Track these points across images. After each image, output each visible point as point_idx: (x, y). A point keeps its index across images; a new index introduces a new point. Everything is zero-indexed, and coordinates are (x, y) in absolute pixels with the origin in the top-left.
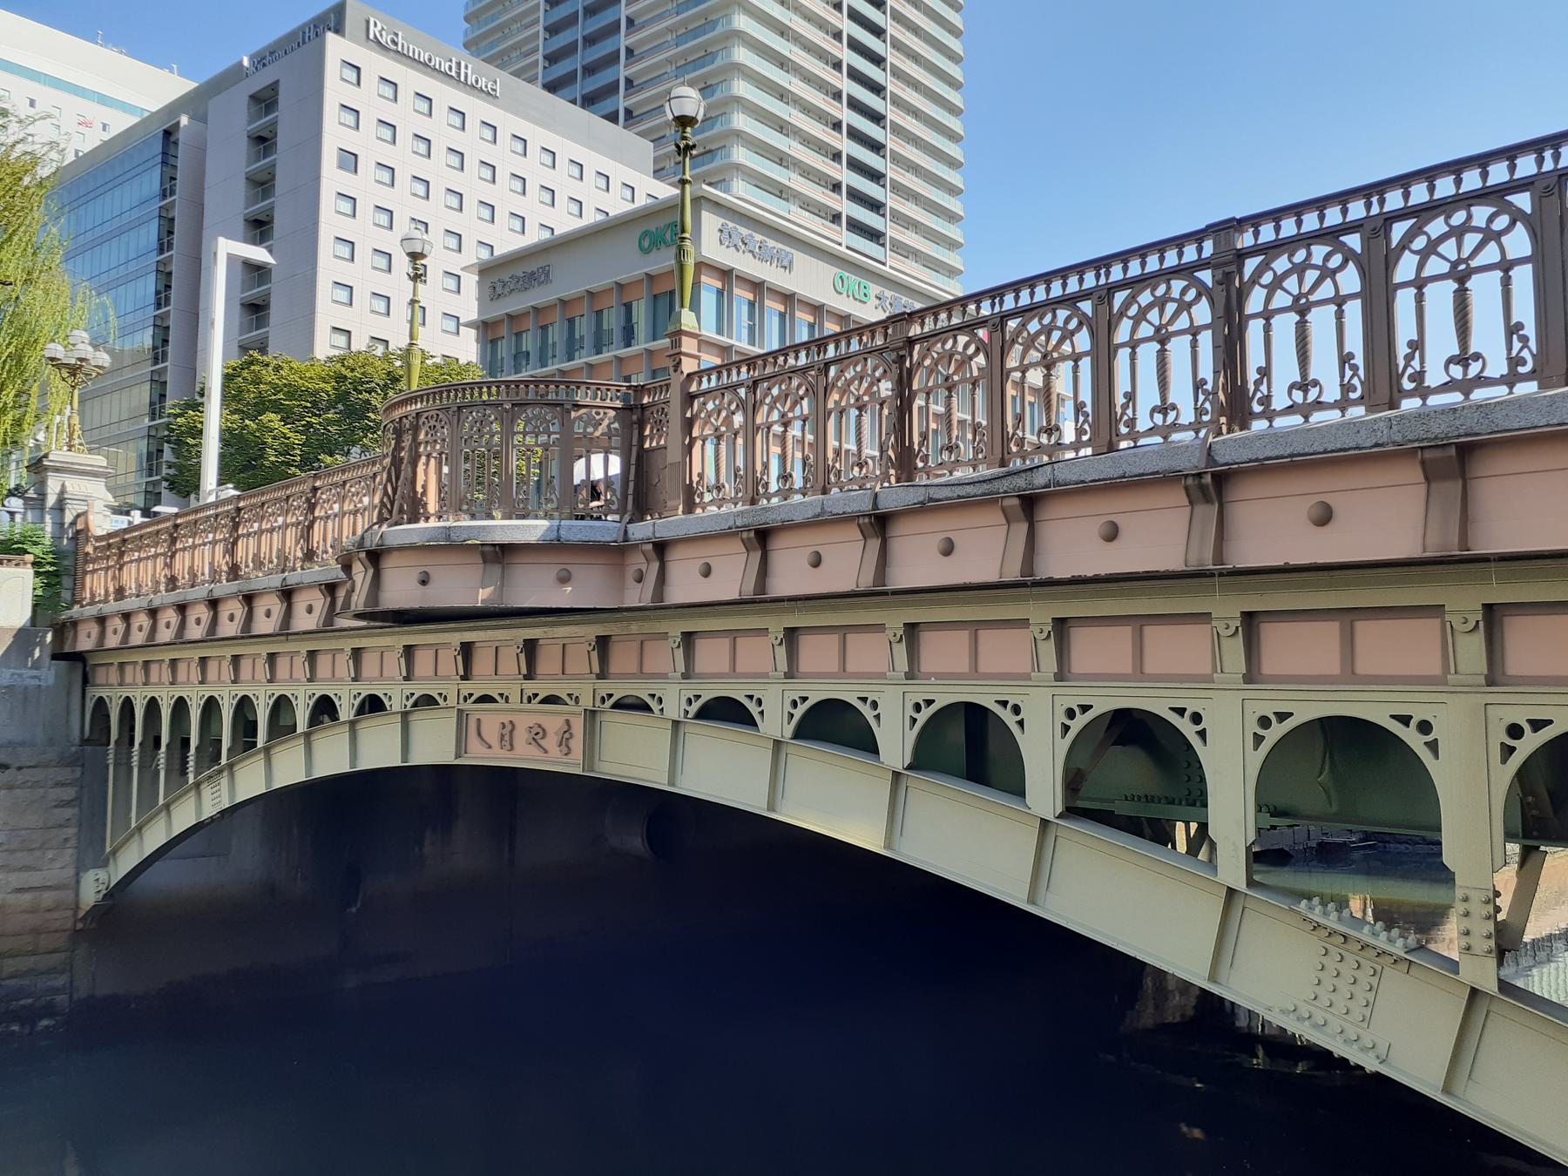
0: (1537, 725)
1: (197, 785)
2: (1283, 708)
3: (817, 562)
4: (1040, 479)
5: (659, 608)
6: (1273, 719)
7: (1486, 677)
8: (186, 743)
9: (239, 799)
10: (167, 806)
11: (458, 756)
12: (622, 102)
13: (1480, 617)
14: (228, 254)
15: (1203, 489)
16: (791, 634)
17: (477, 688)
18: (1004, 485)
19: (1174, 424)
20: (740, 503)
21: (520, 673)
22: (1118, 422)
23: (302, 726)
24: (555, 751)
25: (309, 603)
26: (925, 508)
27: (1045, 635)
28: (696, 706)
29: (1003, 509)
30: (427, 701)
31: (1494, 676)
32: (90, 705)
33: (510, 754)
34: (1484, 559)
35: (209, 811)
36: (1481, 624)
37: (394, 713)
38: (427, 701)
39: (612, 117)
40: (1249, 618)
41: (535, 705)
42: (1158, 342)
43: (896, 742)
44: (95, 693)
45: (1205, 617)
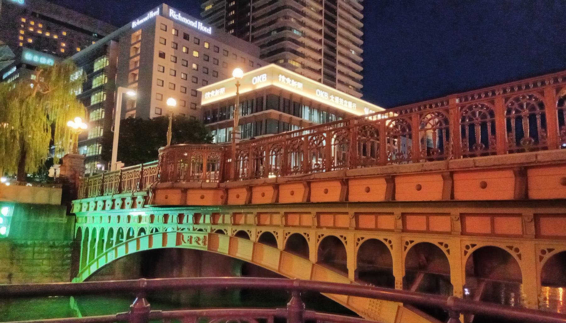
0: (550, 250)
1: (106, 253)
2: (412, 239)
3: (368, 190)
4: (312, 177)
5: (452, 202)
6: (547, 251)
7: (461, 233)
8: (95, 240)
9: (118, 257)
10: (97, 259)
11: (177, 245)
12: (249, 34)
13: (459, 217)
14: (184, 33)
15: (343, 182)
16: (404, 215)
17: (198, 227)
18: (304, 178)
19: (402, 159)
20: (303, 172)
21: (255, 223)
22: (387, 157)
23: (136, 236)
24: (202, 245)
25: (367, 186)
26: (288, 183)
27: (399, 218)
28: (235, 233)
29: (303, 184)
30: (220, 232)
31: (538, 235)
32: (76, 229)
33: (190, 245)
34: (313, 203)
35: (109, 261)
36: (533, 220)
37: (160, 233)
38: (220, 232)
39: (247, 39)
40: (403, 214)
41: (196, 232)
42: (433, 130)
43: (281, 242)
44: (78, 225)
45: (448, 214)
